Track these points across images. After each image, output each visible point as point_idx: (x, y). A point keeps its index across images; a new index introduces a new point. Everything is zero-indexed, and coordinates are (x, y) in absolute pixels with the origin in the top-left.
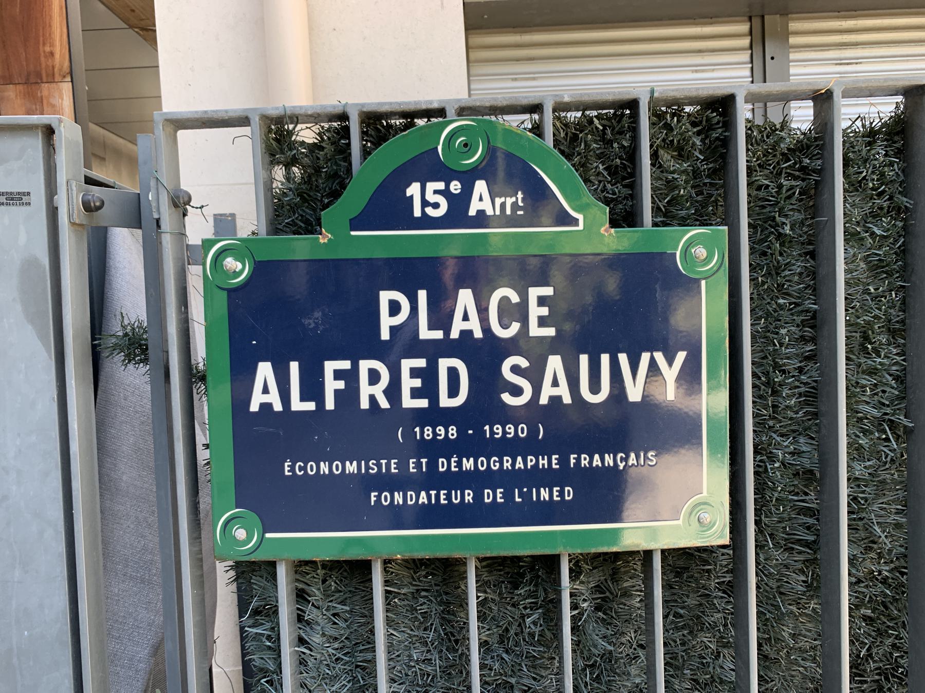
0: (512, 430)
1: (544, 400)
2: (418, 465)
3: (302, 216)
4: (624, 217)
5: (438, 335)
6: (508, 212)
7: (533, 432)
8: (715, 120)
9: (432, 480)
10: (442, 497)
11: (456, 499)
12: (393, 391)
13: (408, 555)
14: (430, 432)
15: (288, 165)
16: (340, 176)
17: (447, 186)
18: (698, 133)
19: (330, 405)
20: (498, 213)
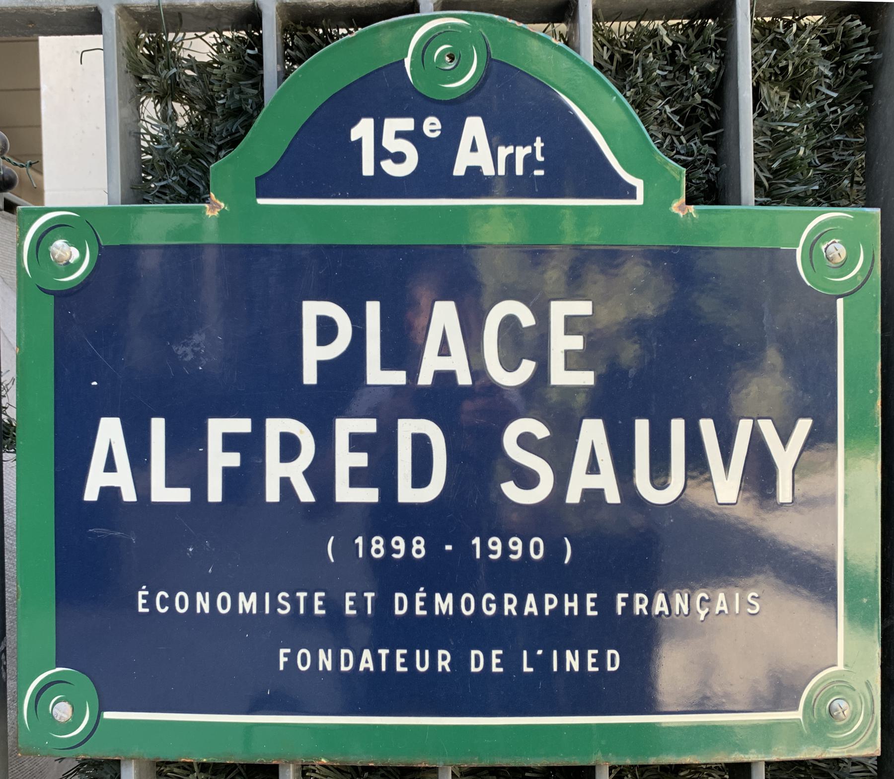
0: (519, 548)
1: (573, 496)
2: (360, 603)
3: (183, 179)
4: (711, 189)
5: (399, 378)
6: (519, 171)
7: (554, 550)
8: (858, 33)
9: (386, 630)
10: (399, 660)
11: (422, 664)
12: (321, 474)
13: (338, 760)
14: (380, 546)
15: (162, 98)
16: (246, 112)
17: (419, 125)
18: (827, 56)
19: (215, 494)
20: (502, 171)
